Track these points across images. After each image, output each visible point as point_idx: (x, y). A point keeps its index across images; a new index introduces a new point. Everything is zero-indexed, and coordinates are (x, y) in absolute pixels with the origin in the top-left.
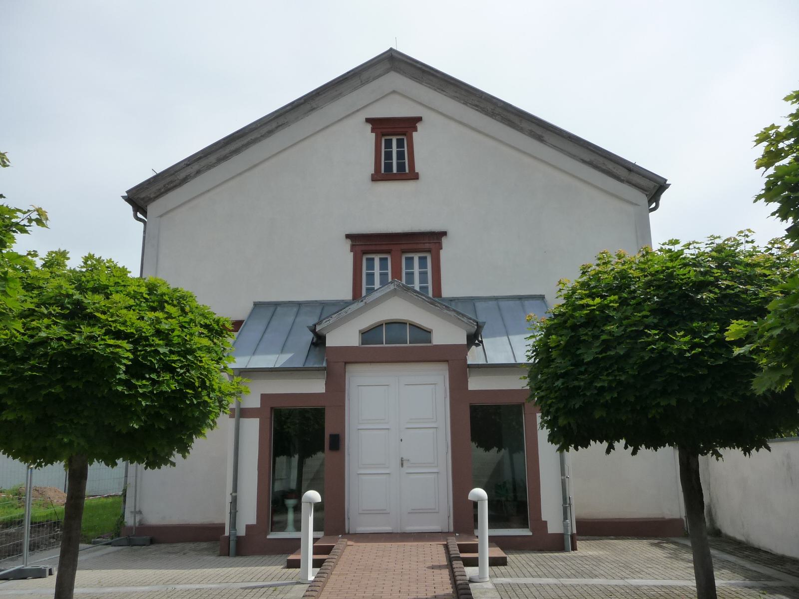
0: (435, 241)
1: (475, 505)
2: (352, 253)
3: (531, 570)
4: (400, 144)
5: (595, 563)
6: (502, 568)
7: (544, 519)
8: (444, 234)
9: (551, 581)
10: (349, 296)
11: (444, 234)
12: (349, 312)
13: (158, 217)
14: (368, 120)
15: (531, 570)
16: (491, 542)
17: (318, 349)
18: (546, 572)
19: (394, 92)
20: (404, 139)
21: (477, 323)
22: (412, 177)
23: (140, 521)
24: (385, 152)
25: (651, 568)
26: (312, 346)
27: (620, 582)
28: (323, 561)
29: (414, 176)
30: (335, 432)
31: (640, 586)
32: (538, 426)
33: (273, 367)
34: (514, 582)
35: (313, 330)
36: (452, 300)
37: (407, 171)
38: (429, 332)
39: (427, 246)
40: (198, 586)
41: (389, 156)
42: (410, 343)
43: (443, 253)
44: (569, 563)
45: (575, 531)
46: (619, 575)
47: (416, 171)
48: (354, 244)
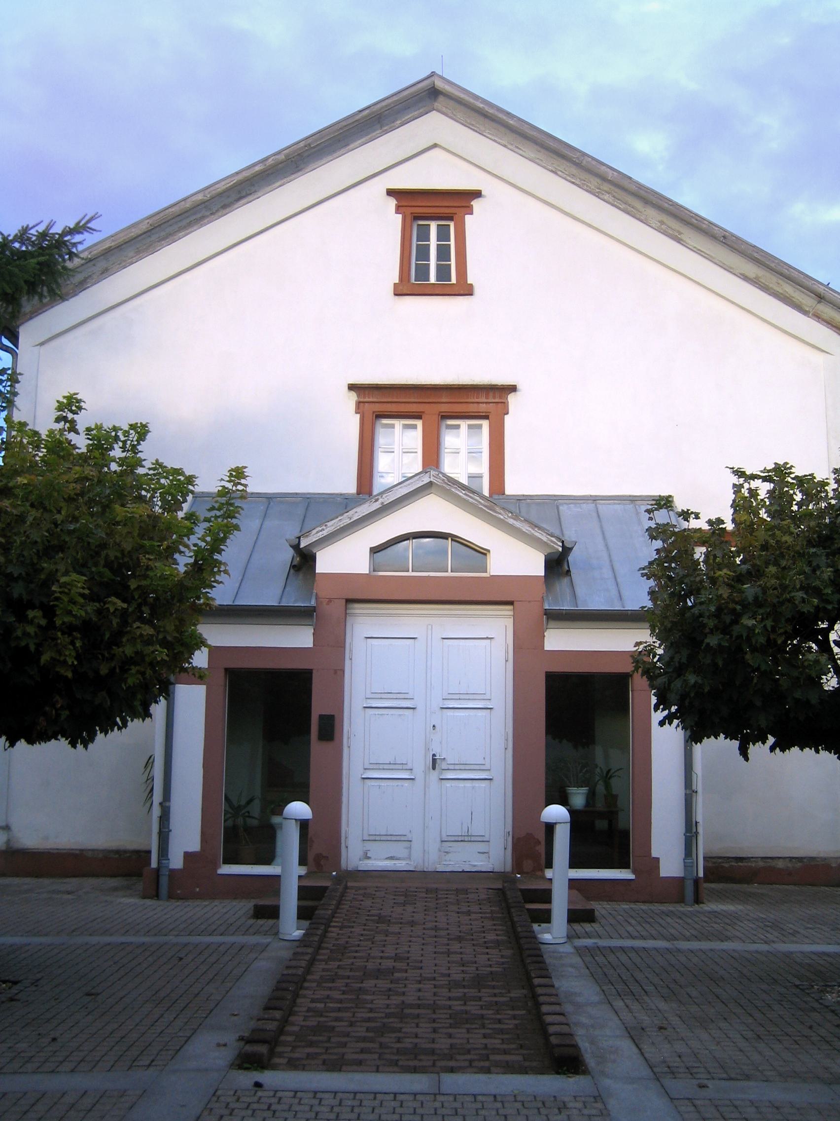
0: (497, 400)
1: (550, 828)
2: (358, 416)
3: (630, 929)
4: (443, 234)
5: (728, 921)
6: (588, 927)
7: (654, 854)
8: (513, 389)
9: (661, 944)
10: (351, 487)
11: (513, 389)
12: (355, 518)
13: (37, 345)
14: (391, 193)
15: (630, 929)
16: (571, 889)
17: (301, 575)
18: (654, 932)
19: (435, 146)
20: (449, 225)
21: (563, 542)
22: (462, 292)
23: (8, 842)
24: (417, 245)
25: (811, 928)
26: (292, 571)
27: (764, 947)
28: (314, 908)
29: (465, 290)
30: (326, 712)
31: (792, 953)
32: (652, 710)
33: (231, 603)
34: (604, 945)
35: (296, 547)
36: (520, 499)
37: (454, 280)
38: (483, 553)
39: (483, 408)
40: (123, 939)
41: (423, 252)
42: (452, 572)
43: (509, 421)
44: (690, 921)
45: (701, 874)
46: (762, 937)
47: (469, 282)
48: (362, 400)
